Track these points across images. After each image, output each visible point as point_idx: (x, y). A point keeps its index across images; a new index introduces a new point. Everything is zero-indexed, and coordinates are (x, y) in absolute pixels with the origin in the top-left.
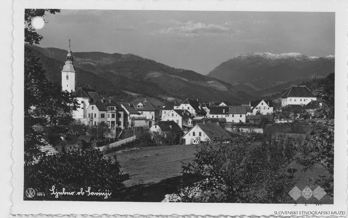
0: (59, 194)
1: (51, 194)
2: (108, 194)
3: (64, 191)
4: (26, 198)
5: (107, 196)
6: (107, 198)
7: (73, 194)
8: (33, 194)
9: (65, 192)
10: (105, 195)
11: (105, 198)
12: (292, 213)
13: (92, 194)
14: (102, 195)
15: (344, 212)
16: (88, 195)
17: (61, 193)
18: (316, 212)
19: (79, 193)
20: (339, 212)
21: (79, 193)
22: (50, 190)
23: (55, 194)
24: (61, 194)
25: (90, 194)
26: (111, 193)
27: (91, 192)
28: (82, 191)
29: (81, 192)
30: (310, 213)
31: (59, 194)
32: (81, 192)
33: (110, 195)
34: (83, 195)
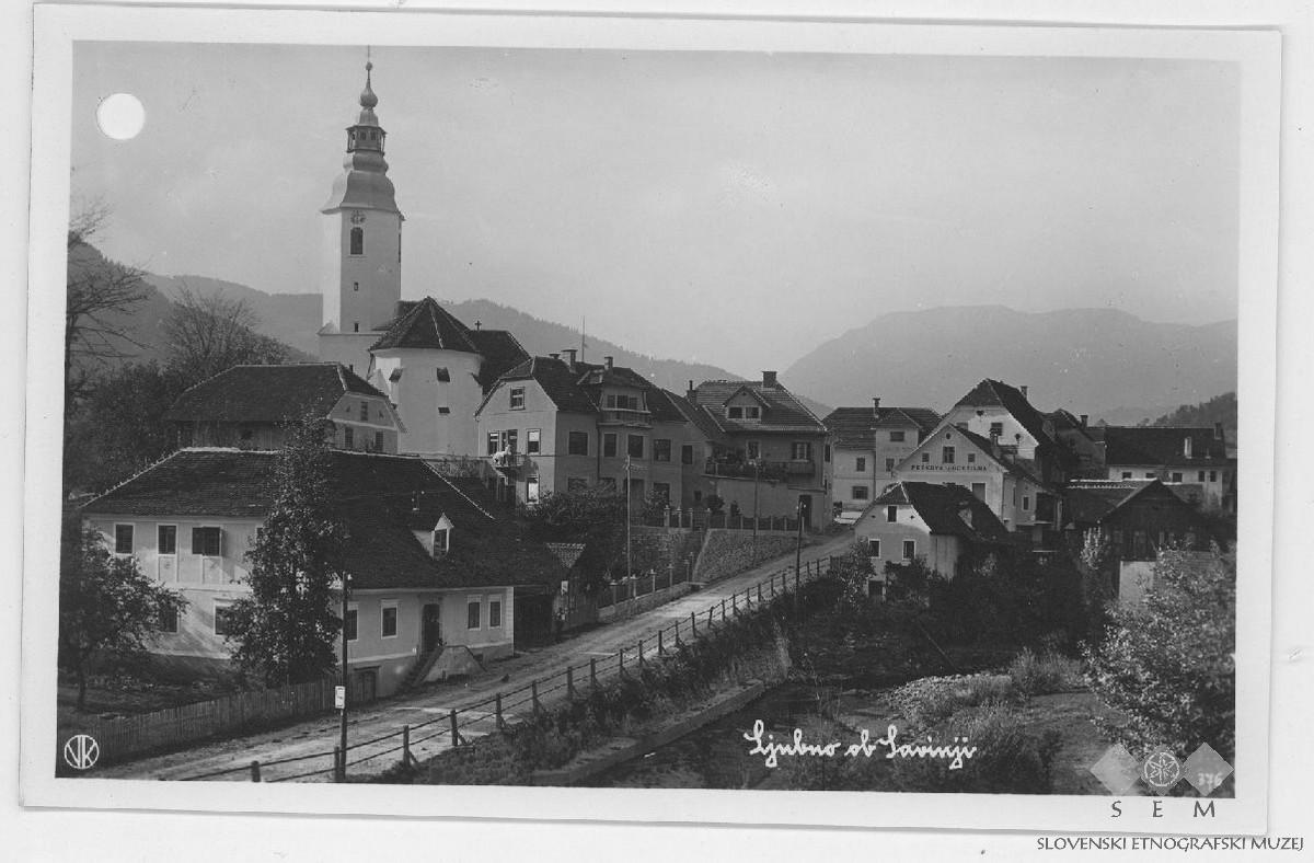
0: (793, 748)
1: (752, 752)
2: (965, 750)
3: (797, 740)
4: (64, 770)
5: (959, 759)
6: (960, 766)
7: (831, 754)
8: (93, 755)
9: (804, 745)
10: (951, 755)
11: (952, 767)
12: (1103, 845)
13: (902, 752)
14: (942, 755)
15: (1299, 841)
16: (889, 756)
17: (785, 750)
18: (1194, 841)
19: (854, 750)
20: (1282, 842)
21: (854, 750)
22: (746, 736)
23: (765, 752)
24: (817, 753)
25: (895, 752)
26: (974, 749)
27: (900, 741)
28: (864, 741)
29: (863, 745)
30: (1170, 843)
31: (779, 751)
32: (863, 745)
33: (969, 755)
34: (868, 754)
